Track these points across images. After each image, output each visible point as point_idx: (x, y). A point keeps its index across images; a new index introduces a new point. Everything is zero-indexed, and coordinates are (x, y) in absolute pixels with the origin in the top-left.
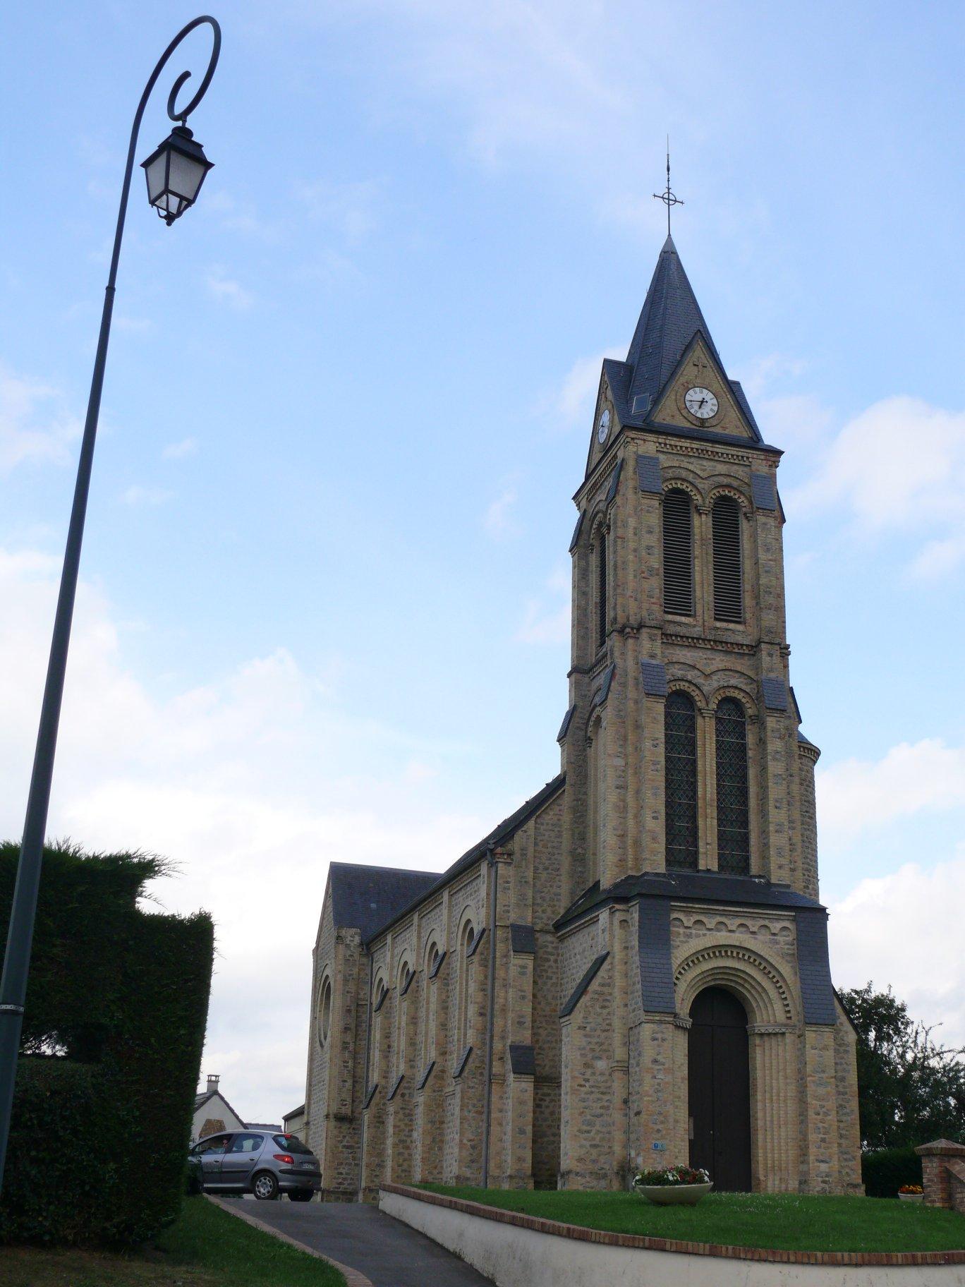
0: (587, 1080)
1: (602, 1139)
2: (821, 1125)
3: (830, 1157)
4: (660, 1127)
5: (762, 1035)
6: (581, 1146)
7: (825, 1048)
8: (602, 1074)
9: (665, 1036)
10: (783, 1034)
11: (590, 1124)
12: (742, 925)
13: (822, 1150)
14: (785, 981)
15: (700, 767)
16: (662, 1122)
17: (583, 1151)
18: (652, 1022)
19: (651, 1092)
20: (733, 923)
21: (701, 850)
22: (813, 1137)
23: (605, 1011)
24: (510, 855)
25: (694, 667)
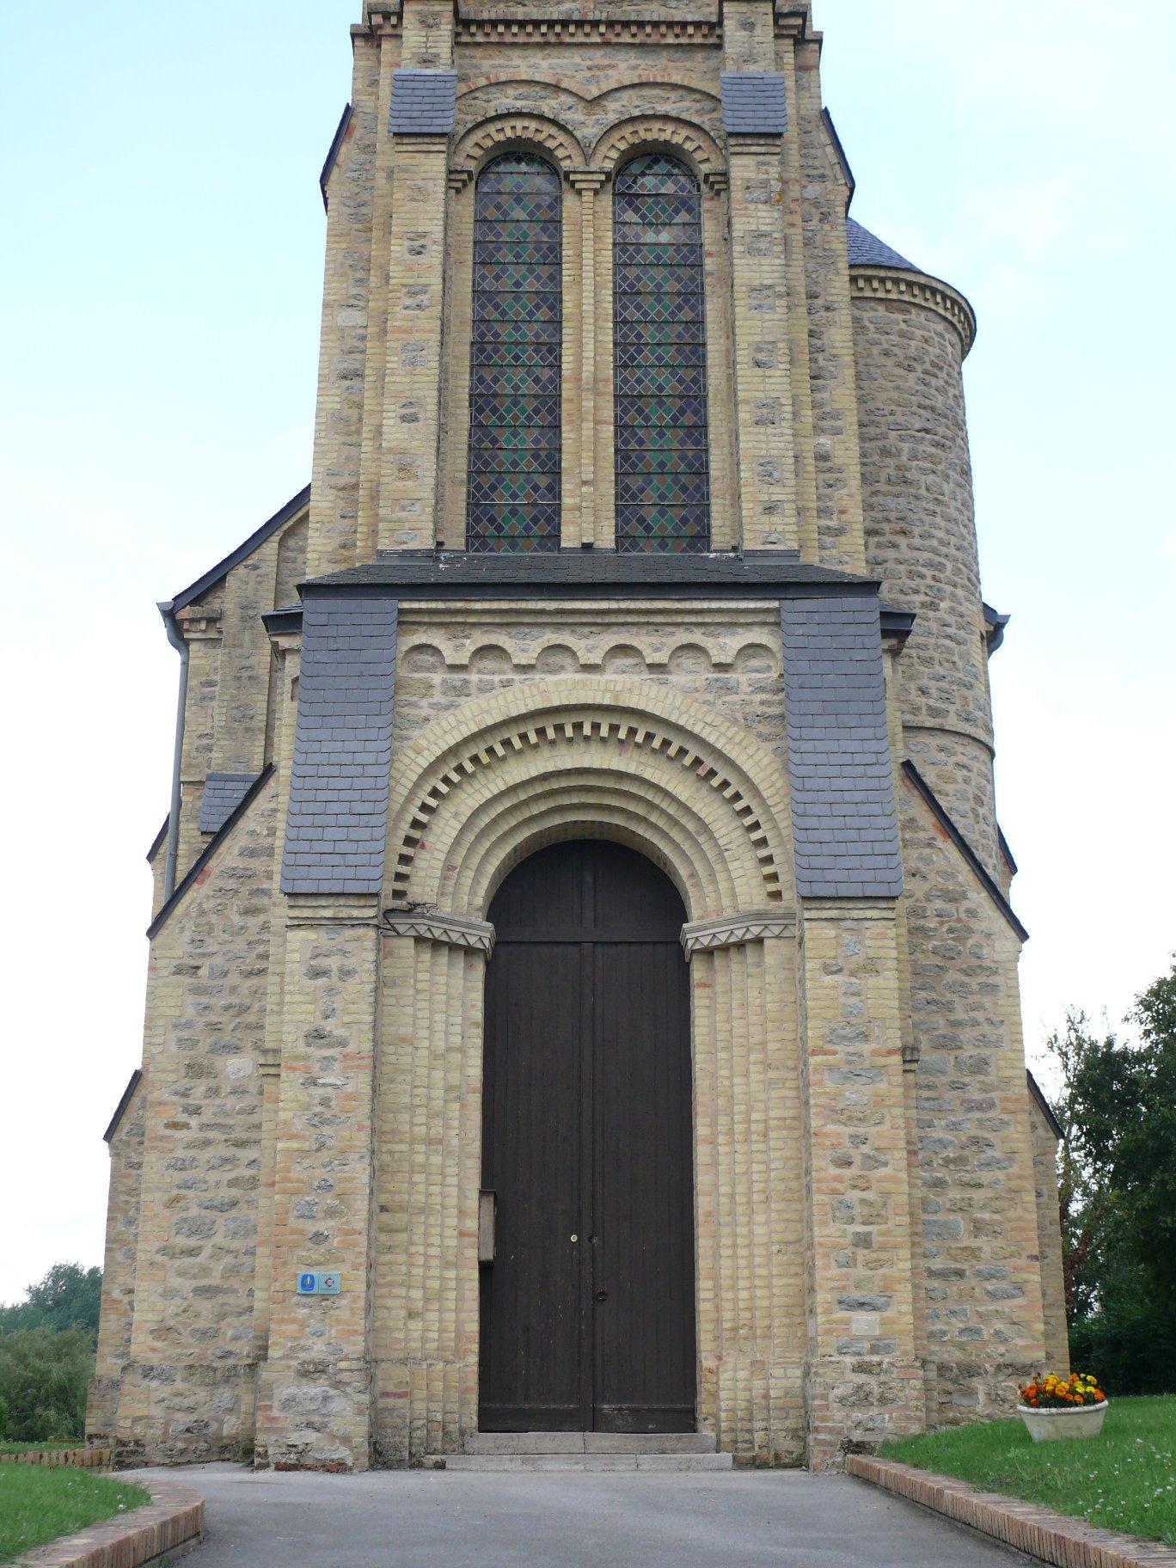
0: (196, 1111)
1: (233, 1271)
2: (854, 1195)
3: (887, 1292)
4: (322, 1226)
5: (709, 952)
6: (168, 1294)
7: (870, 967)
8: (239, 1091)
9: (350, 963)
10: (759, 941)
11: (199, 1229)
12: (623, 649)
13: (861, 1271)
14: (756, 793)
15: (568, 306)
16: (331, 1213)
17: (173, 1306)
18: (313, 924)
19: (299, 1125)
20: (591, 647)
21: (567, 501)
22: (827, 1232)
23: (254, 922)
24: (212, 621)
25: (556, 88)
